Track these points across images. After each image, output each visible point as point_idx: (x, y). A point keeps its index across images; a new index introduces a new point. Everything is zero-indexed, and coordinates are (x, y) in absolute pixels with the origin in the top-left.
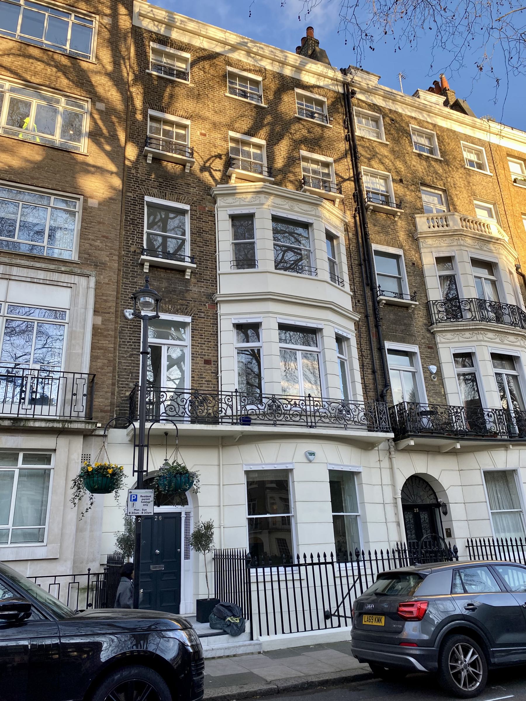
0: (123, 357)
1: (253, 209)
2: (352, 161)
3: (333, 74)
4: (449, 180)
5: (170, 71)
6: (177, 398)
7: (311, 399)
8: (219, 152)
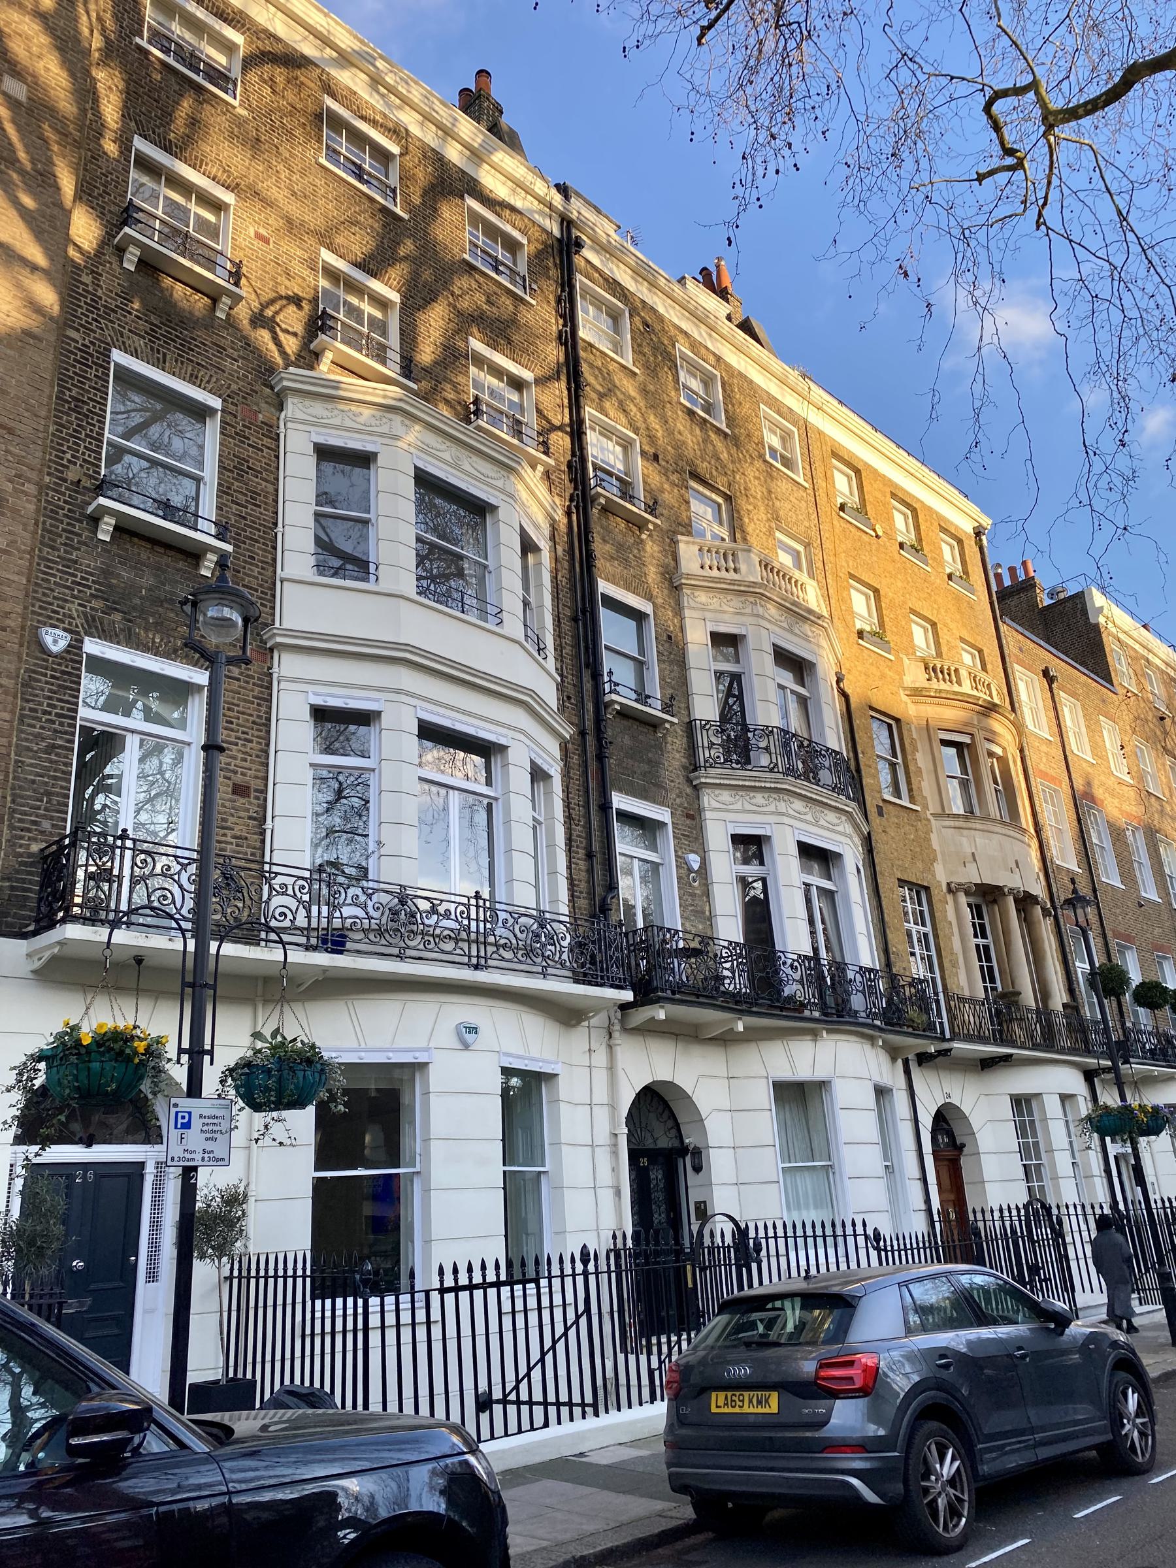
0: (28, 749)
1: (374, 443)
2: (569, 389)
3: (545, 190)
4: (738, 477)
5: (192, 60)
6: (179, 873)
7: (481, 903)
8: (296, 290)
